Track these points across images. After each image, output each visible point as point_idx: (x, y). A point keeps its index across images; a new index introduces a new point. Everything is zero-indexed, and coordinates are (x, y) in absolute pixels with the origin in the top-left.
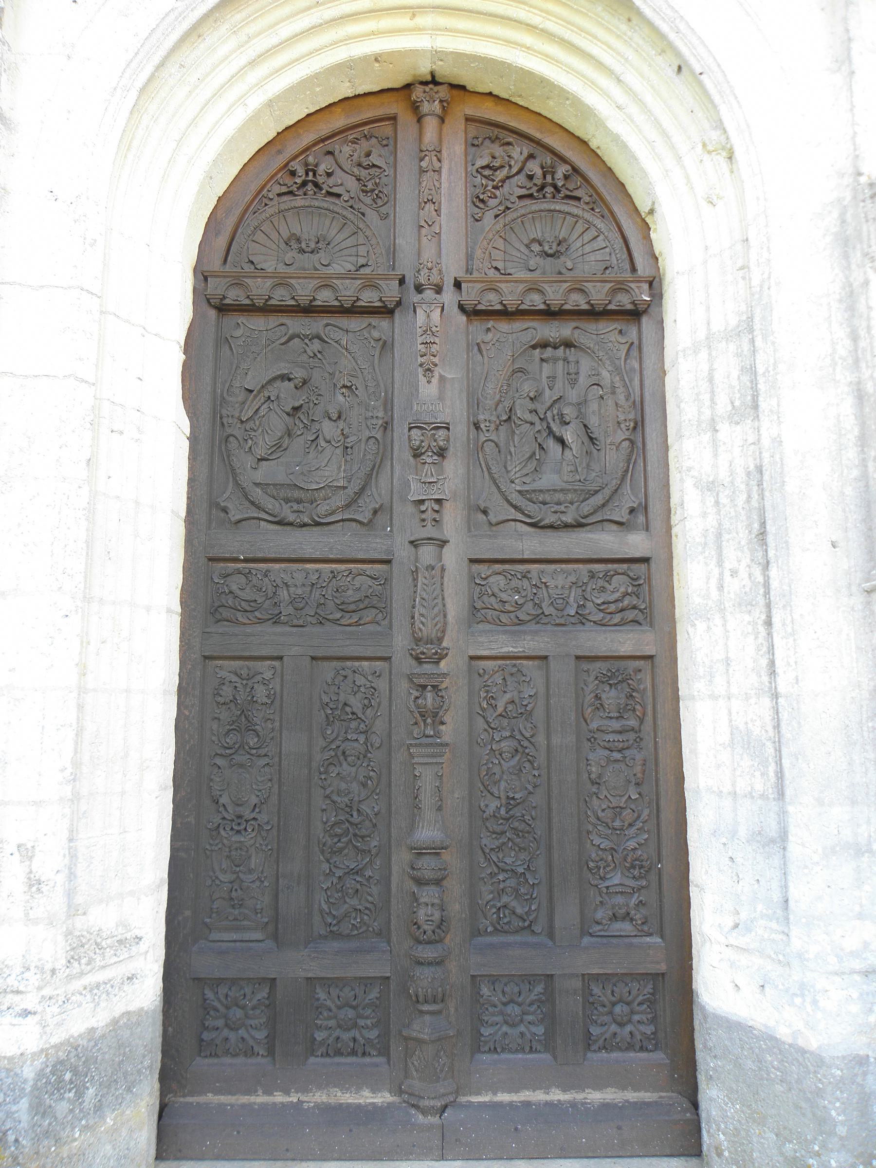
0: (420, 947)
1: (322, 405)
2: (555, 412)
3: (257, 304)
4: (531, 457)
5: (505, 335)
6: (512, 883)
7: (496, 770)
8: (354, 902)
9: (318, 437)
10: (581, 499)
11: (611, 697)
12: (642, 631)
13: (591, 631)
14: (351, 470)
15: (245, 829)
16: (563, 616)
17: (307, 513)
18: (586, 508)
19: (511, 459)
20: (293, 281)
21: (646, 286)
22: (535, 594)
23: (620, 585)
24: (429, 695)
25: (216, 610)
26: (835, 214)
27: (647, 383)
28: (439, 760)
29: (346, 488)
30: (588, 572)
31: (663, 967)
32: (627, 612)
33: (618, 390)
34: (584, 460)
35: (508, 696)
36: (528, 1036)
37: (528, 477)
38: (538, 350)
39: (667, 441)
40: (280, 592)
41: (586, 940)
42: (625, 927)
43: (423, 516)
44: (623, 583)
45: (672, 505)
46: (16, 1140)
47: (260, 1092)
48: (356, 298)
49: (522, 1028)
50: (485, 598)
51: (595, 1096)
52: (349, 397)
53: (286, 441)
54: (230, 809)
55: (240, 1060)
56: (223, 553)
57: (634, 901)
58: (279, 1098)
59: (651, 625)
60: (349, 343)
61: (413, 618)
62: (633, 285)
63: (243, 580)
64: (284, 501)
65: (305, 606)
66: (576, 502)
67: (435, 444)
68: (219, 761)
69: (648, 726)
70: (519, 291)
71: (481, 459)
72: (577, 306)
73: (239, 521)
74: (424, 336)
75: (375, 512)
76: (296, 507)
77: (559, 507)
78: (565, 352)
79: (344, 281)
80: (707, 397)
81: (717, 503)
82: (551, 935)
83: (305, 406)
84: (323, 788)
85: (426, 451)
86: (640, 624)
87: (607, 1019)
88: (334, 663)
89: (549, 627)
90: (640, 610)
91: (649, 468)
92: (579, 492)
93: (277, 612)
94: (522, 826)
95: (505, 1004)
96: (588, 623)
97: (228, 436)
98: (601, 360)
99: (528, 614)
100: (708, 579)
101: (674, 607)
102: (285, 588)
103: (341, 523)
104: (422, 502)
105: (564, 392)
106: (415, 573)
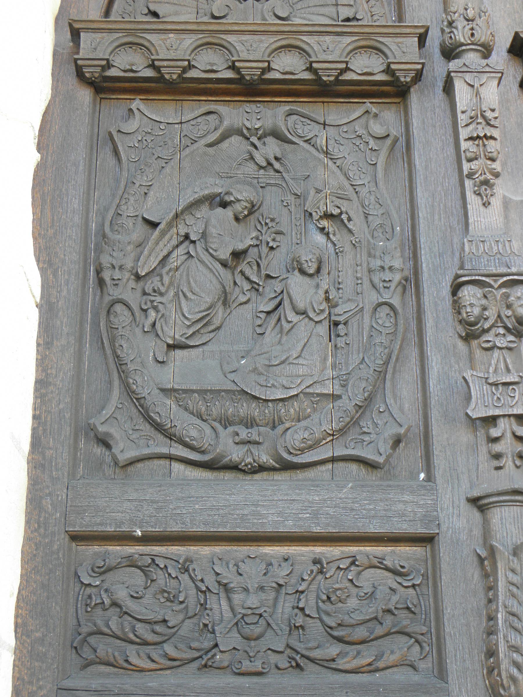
1: (283, 250)
3: (167, 77)
9: (280, 304)
14: (347, 364)
17: (266, 444)
25: (85, 640)
29: (339, 397)
40: (212, 602)
43: (497, 448)
48: (343, 66)
52: (334, 235)
53: (220, 313)
56: (101, 524)
60: (331, 142)
61: (491, 653)
64: (220, 422)
65: (265, 631)
67: (509, 313)
73: (132, 463)
74: (471, 127)
75: (397, 441)
76: (244, 433)
79: (322, 38)
83: (253, 252)
85: (492, 326)
93: (207, 644)
97: (113, 303)
102: (222, 595)
103: (330, 466)
104: (492, 420)
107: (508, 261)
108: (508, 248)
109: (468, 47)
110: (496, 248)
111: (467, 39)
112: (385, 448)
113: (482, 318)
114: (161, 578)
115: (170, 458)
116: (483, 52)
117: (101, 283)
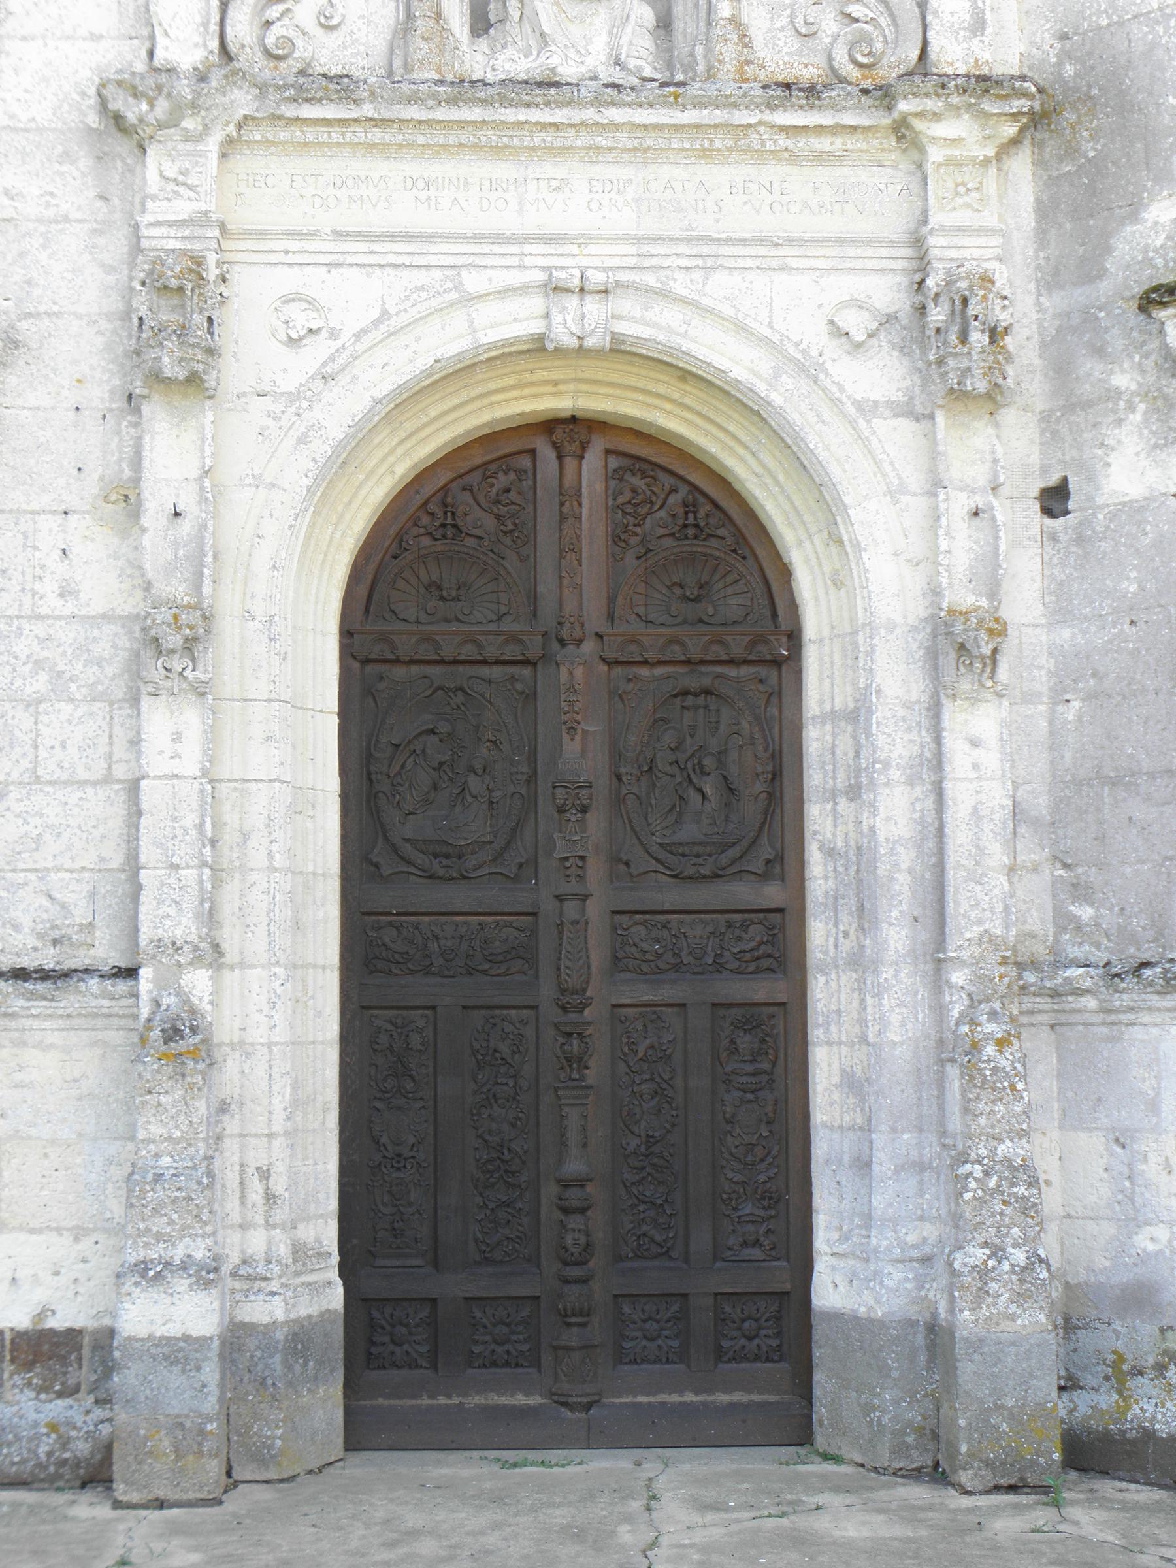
0: (568, 1268)
2: (696, 761)
4: (670, 810)
6: (652, 1213)
7: (637, 1110)
8: (507, 1231)
11: (745, 1042)
15: (405, 1167)
18: (724, 860)
20: (437, 638)
23: (756, 933)
24: (575, 1042)
26: (928, 630)
28: (584, 1101)
31: (787, 1287)
32: (762, 961)
35: (648, 1042)
36: (665, 1348)
40: (430, 944)
41: (719, 1264)
42: (756, 1253)
46: (274, 1384)
47: (425, 1397)
49: (660, 1342)
50: (627, 948)
51: (724, 1398)
54: (389, 1148)
55: (405, 1372)
57: (762, 1230)
58: (442, 1400)
59: (785, 974)
61: (559, 969)
62: (771, 638)
63: (394, 932)
68: (379, 1105)
69: (779, 1069)
76: (445, 862)
80: (829, 767)
81: (835, 870)
82: (687, 1260)
84: (476, 1129)
87: (735, 1333)
88: (483, 1012)
89: (688, 976)
90: (775, 959)
93: (428, 963)
94: (661, 1162)
95: (644, 1321)
100: (828, 936)
104: (567, 859)
106: (560, 926)
112: (514, 869)
113: (564, 805)
114: (405, 933)
115: (408, 873)
117: (370, 780)
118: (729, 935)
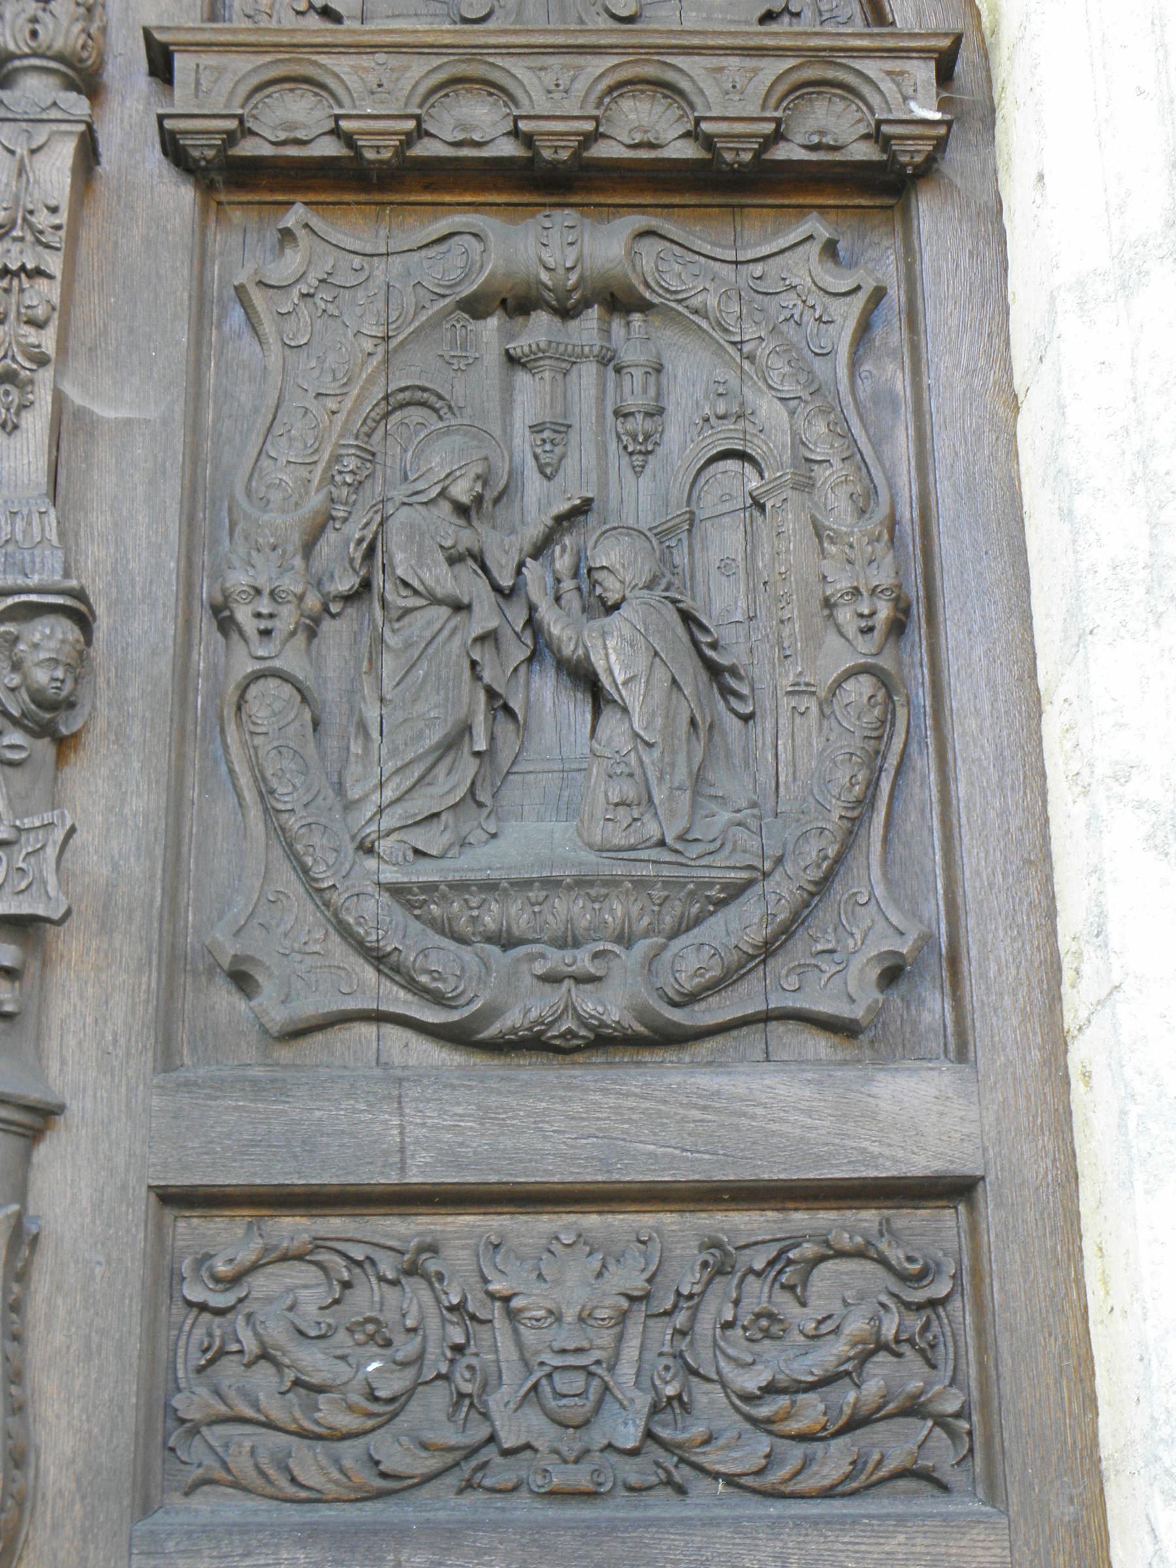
2: (563, 562)
5: (357, 261)
10: (668, 921)
12: (946, 1518)
13: (713, 1522)
16: (587, 1451)
19: (366, 749)
21: (924, 72)
22: (458, 1349)
27: (943, 445)
30: (703, 1247)
32: (879, 1433)
33: (822, 474)
34: (681, 759)
37: (435, 827)
38: (493, 322)
39: (1033, 675)
44: (862, 1297)
45: (1064, 943)
59: (993, 1492)
62: (871, 67)
66: (646, 934)
70: (406, 85)
71: (235, 749)
72: (651, 146)
77: (568, 955)
78: (606, 332)
86: (944, 1488)
89: (523, 1508)
90: (941, 1421)
91: (961, 789)
92: (658, 893)
96: (700, 1487)
98: (751, 358)
99: (425, 1446)
101: (1090, 1401)
105: (604, 485)
107: (28, 559)
108: (36, 529)
109: (26, 62)
110: (9, 529)
111: (21, 44)
116: (64, 75)
118: (717, 1308)
